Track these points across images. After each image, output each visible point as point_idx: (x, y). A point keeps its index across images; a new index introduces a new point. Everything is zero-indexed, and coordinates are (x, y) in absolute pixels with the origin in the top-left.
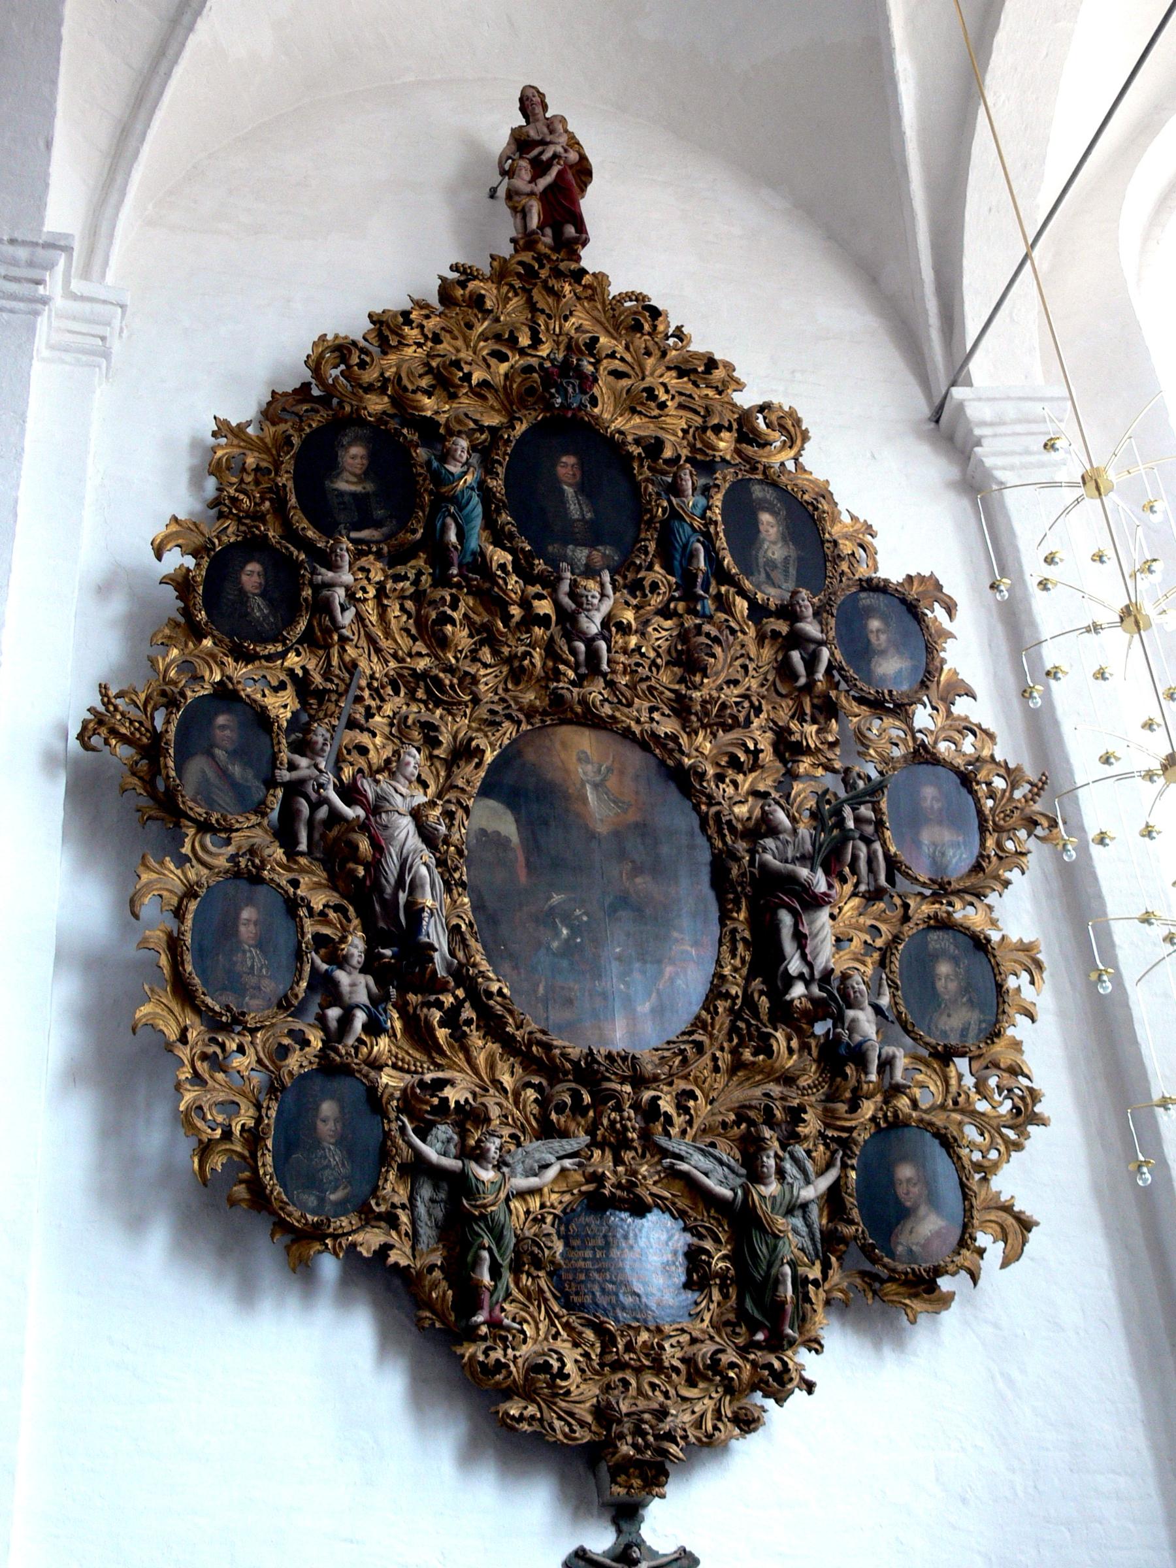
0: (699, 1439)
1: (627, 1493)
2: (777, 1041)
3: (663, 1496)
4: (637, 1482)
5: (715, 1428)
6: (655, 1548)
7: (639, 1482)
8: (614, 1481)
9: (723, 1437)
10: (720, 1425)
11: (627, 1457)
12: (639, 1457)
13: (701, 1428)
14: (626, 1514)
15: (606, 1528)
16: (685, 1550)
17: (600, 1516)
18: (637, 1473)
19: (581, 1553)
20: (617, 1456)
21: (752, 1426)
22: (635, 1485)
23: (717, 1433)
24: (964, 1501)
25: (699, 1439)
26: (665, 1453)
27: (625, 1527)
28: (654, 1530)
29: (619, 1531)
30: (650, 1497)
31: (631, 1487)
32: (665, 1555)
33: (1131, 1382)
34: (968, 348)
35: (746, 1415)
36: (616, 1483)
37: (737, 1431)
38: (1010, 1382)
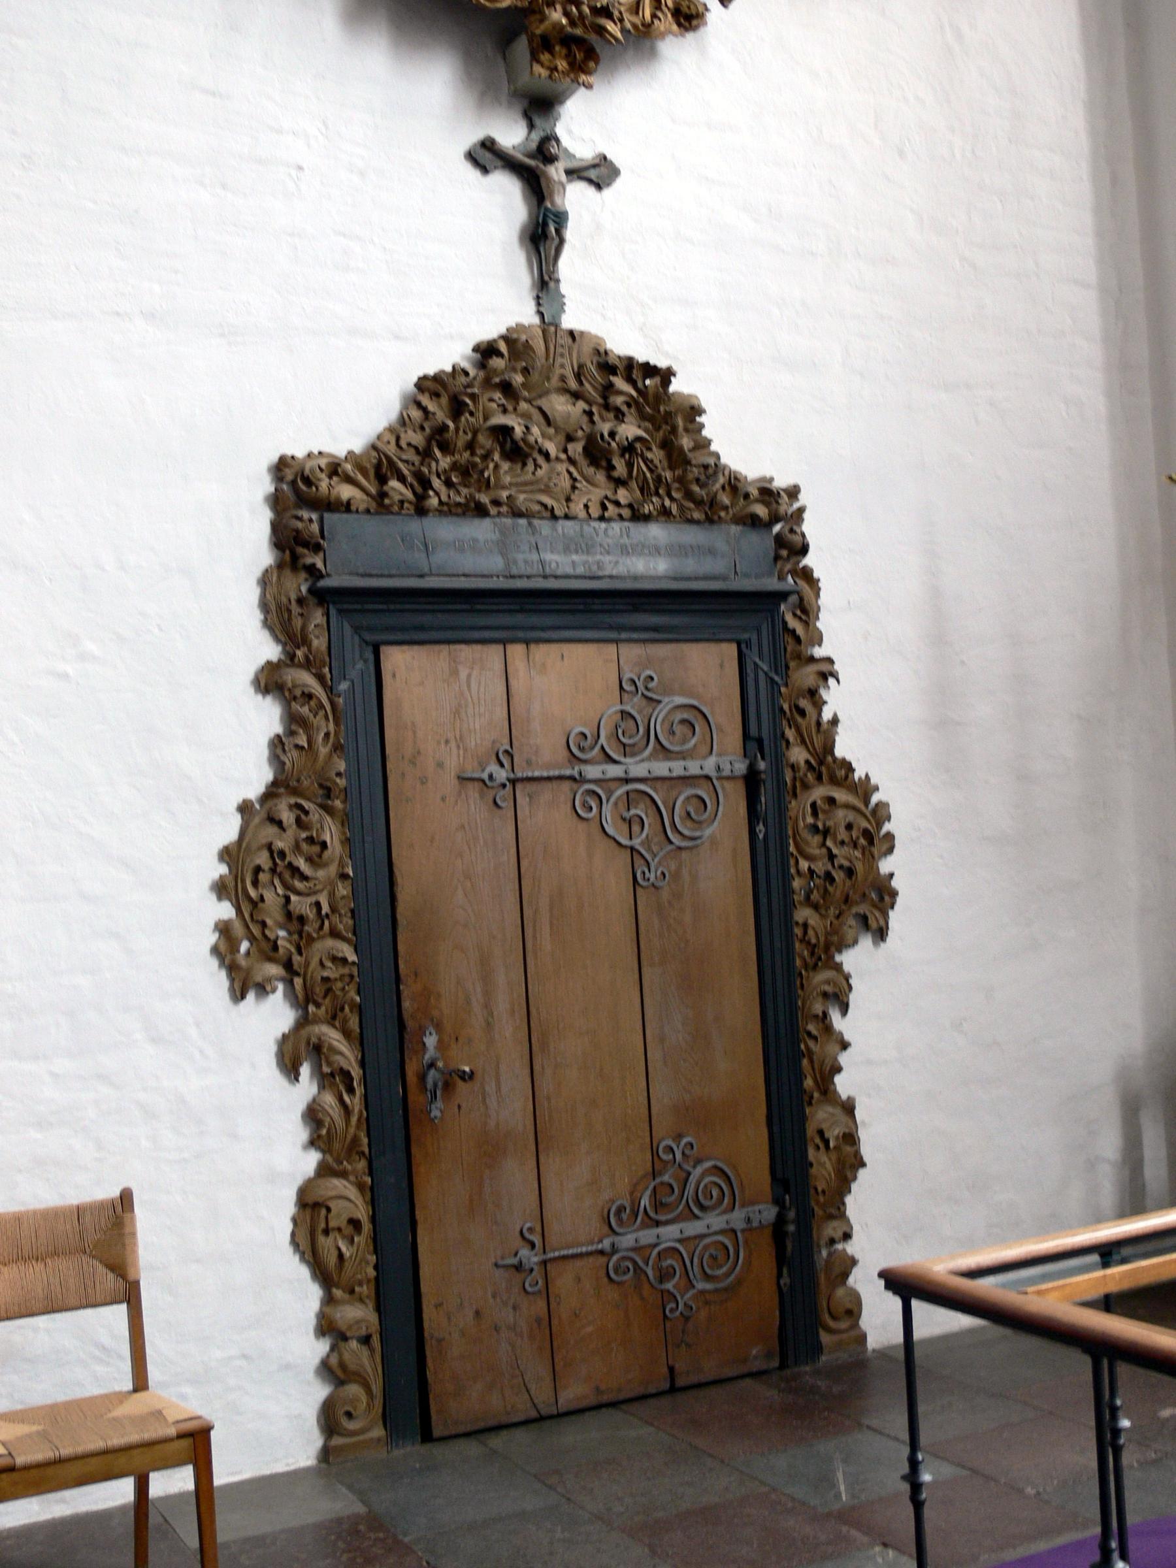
0: (635, 26)
1: (550, 77)
2: (341, 1054)
3: (589, 87)
4: (562, 64)
5: (654, 16)
6: (571, 150)
7: (565, 64)
8: (535, 58)
9: (662, 28)
10: (660, 14)
11: (558, 26)
12: (569, 29)
13: (637, 13)
14: (540, 106)
15: (516, 122)
16: (605, 158)
17: (510, 105)
18: (564, 51)
19: (488, 144)
20: (547, 23)
21: (694, 22)
22: (560, 67)
23: (656, 22)
24: (901, 153)
25: (635, 26)
26: (601, 31)
27: (538, 121)
28: (570, 132)
29: (531, 126)
30: (575, 85)
31: (556, 69)
32: (582, 160)
33: (1087, 219)
34: (964, 1321)
35: (689, 8)
36: (538, 61)
37: (675, 27)
38: (959, 36)
